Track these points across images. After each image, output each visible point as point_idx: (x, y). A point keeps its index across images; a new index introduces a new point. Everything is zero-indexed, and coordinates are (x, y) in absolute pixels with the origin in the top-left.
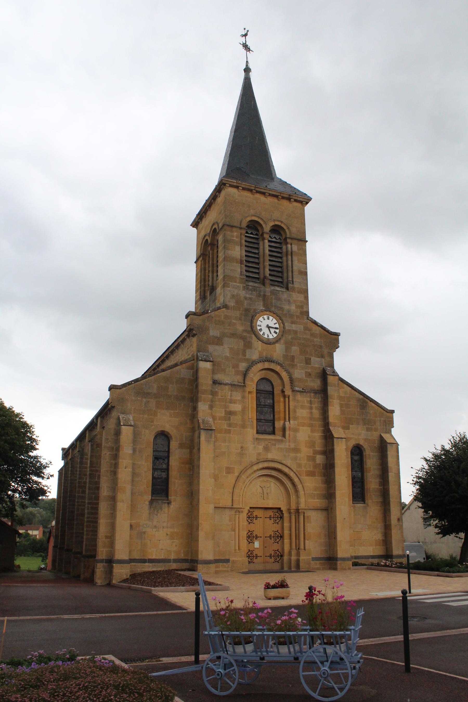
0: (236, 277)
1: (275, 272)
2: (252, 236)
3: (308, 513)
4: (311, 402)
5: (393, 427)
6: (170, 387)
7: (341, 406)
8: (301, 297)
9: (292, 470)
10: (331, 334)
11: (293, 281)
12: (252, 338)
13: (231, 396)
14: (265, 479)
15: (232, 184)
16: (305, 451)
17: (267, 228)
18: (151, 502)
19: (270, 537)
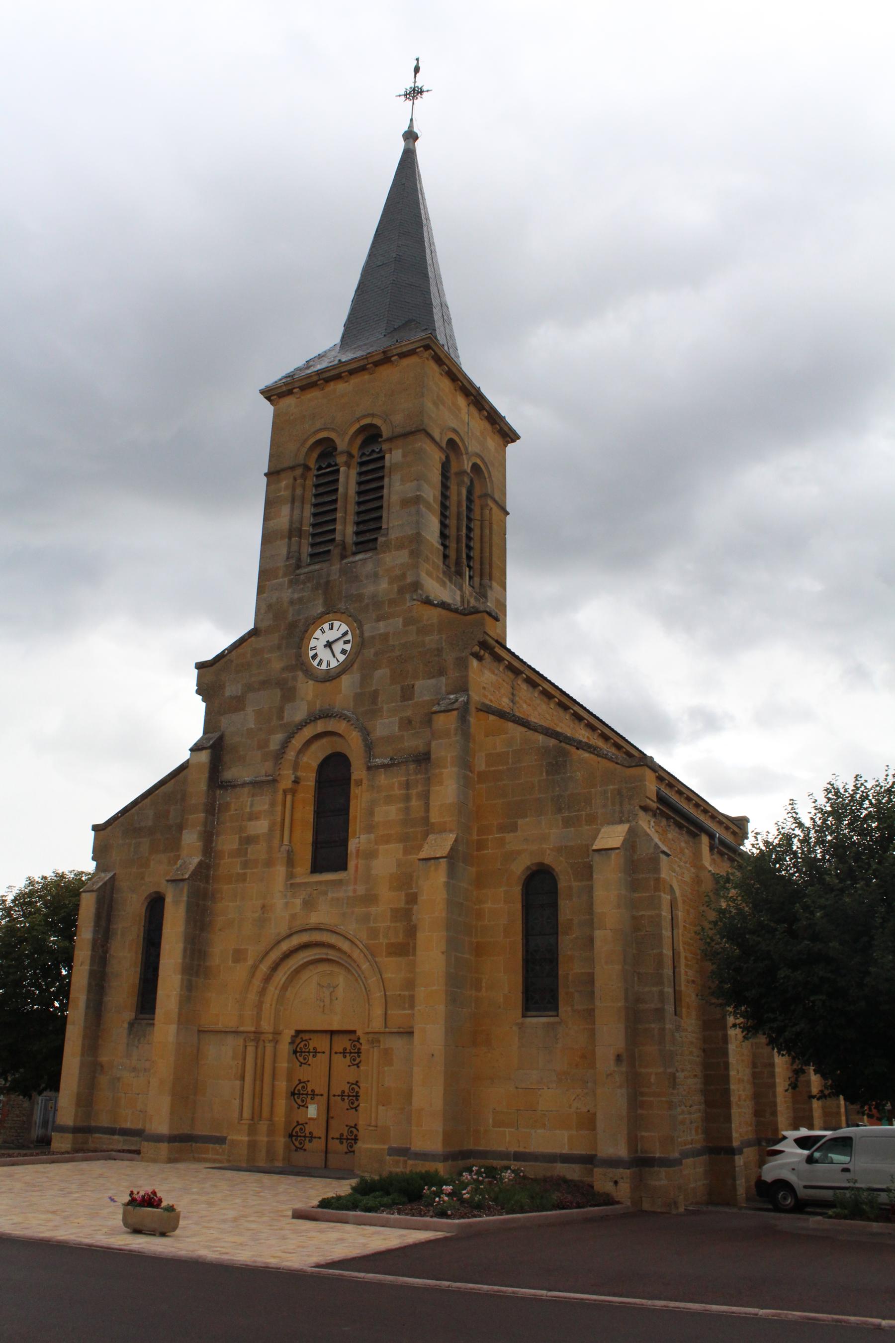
12: (295, 678)
13: (252, 805)
18: (131, 1025)
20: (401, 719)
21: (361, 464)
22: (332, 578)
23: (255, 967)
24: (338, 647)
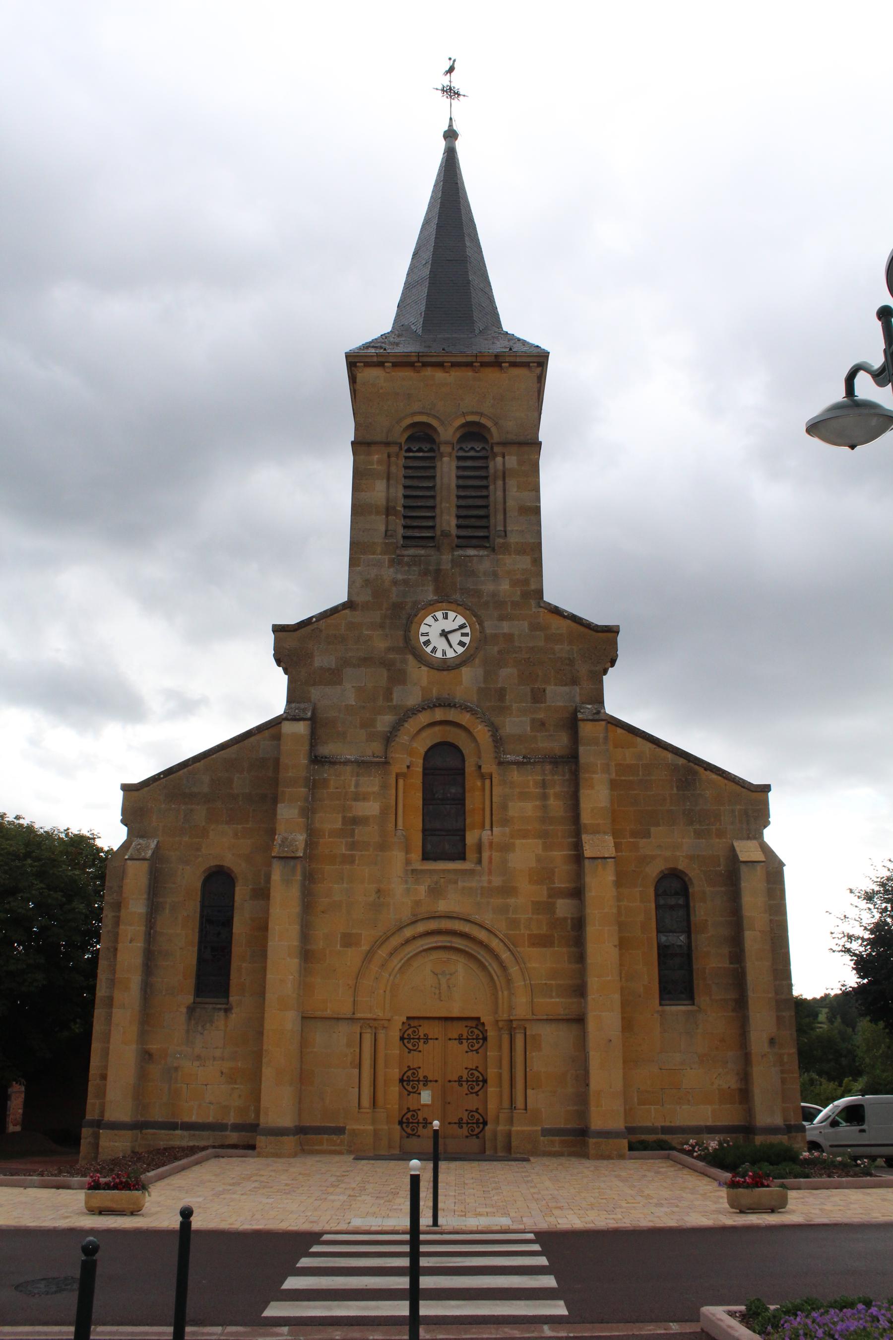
2: (421, 454)
4: (544, 784)
5: (766, 823)
7: (614, 785)
9: (496, 936)
10: (597, 631)
11: (505, 532)
14: (443, 955)
16: (529, 892)
17: (447, 433)
18: (191, 1010)
19: (460, 1081)
21: (459, 458)
22: (443, 567)
23: (369, 956)
24: (455, 638)
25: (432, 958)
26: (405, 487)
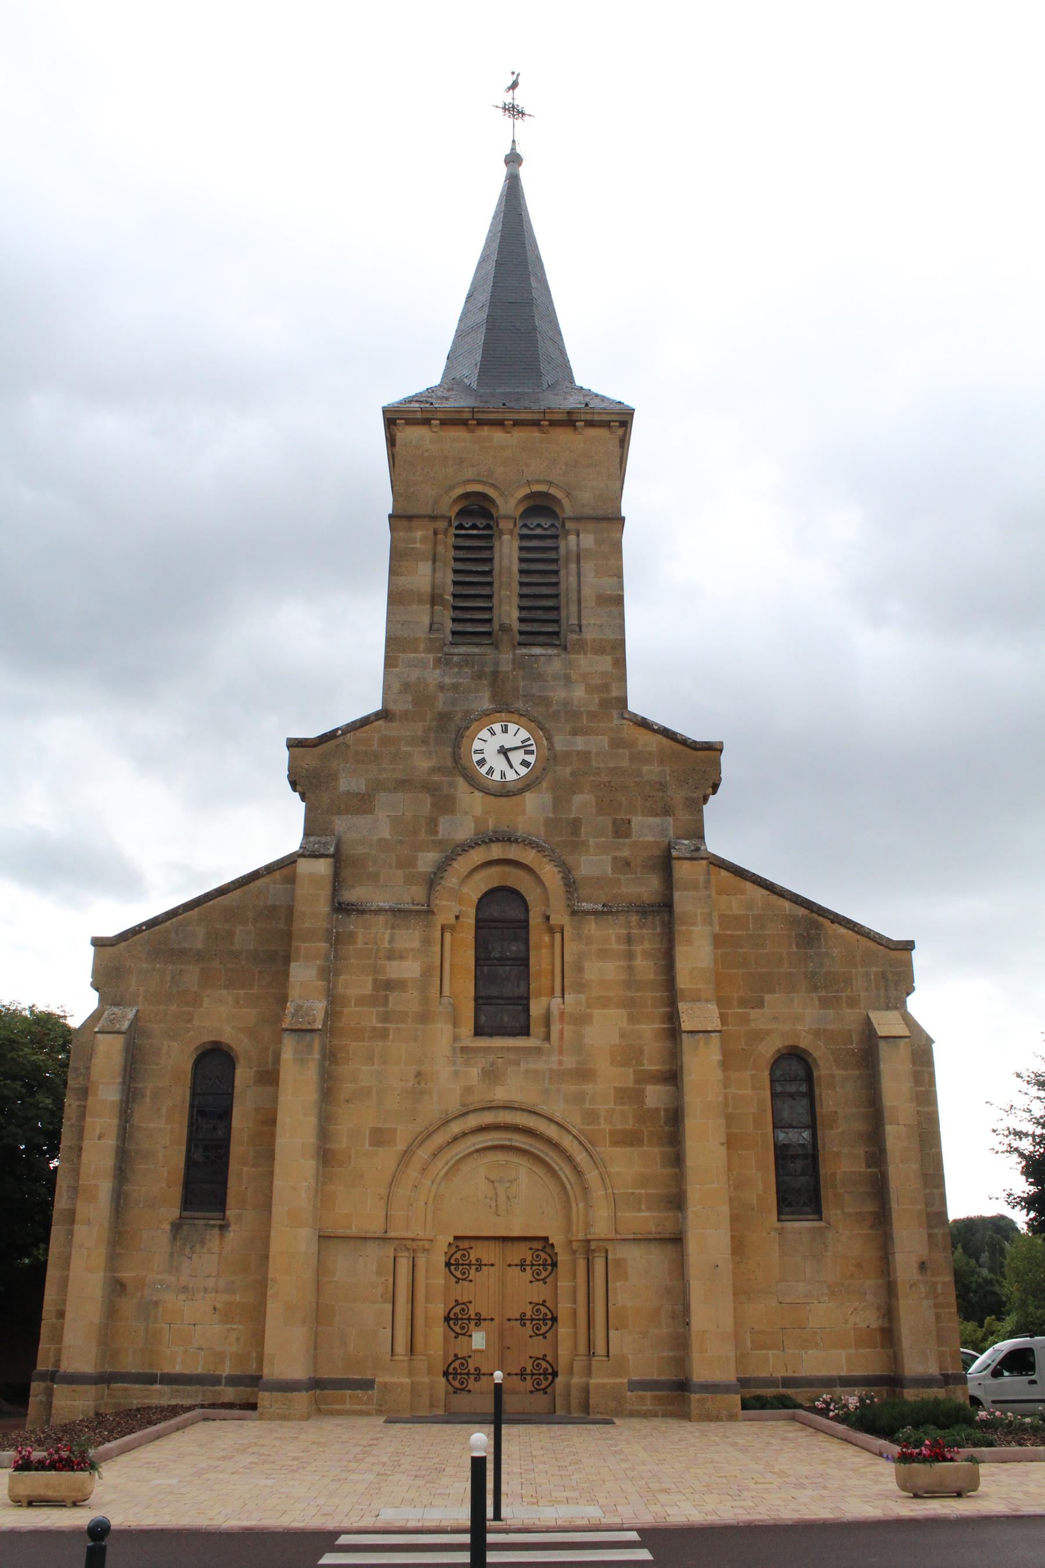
0: (416, 639)
1: (540, 612)
2: (475, 532)
3: (618, 1252)
4: (629, 940)
5: (910, 990)
6: (238, 932)
7: (718, 941)
8: (605, 663)
10: (695, 749)
11: (580, 626)
12: (452, 785)
13: (392, 940)
14: (500, 1157)
15: (411, 416)
16: (611, 1076)
17: (508, 505)
18: (177, 1227)
19: (522, 1319)
20: (615, 858)
21: (522, 537)
23: (406, 1156)
24: (516, 757)
25: (486, 1160)
26: (455, 572)
